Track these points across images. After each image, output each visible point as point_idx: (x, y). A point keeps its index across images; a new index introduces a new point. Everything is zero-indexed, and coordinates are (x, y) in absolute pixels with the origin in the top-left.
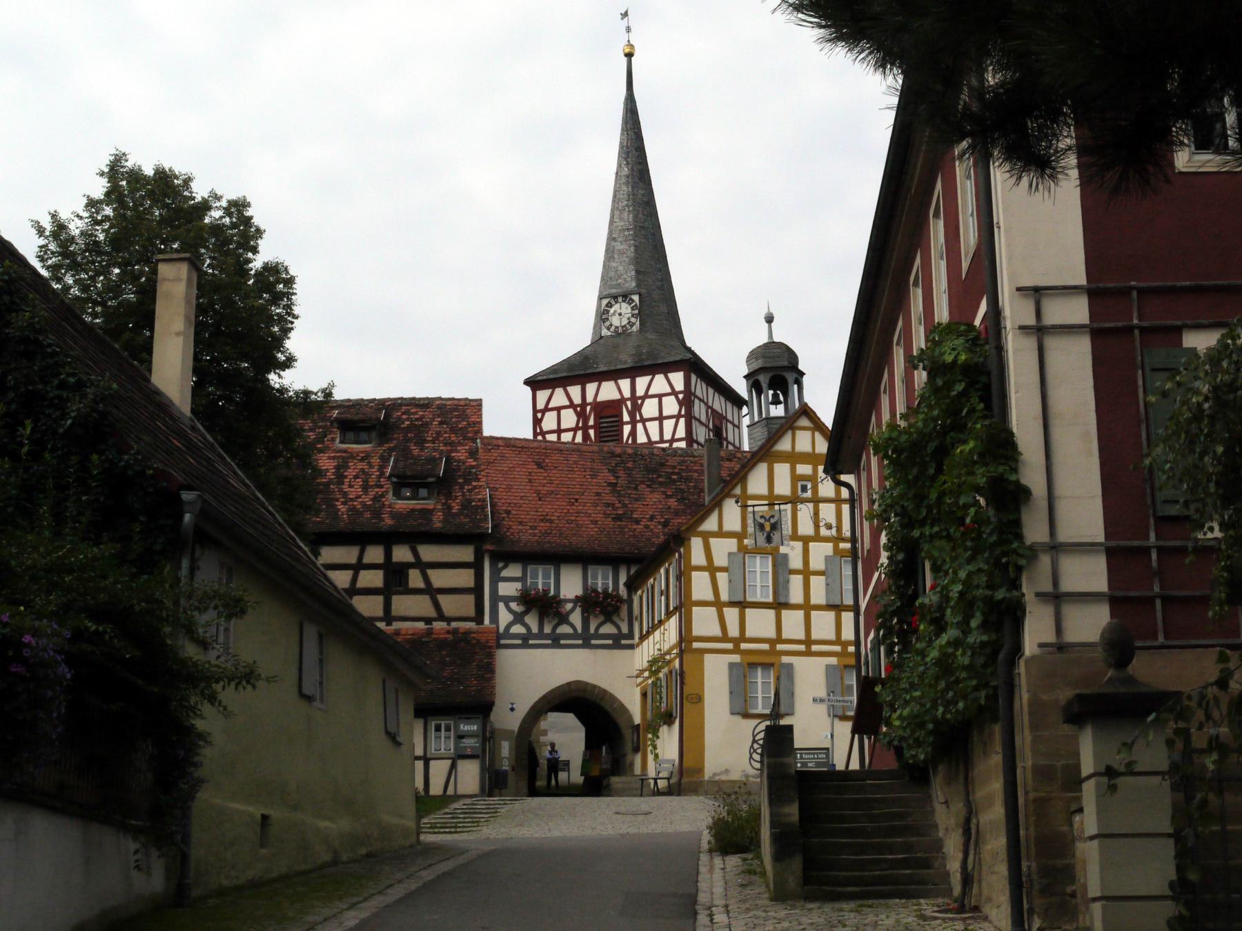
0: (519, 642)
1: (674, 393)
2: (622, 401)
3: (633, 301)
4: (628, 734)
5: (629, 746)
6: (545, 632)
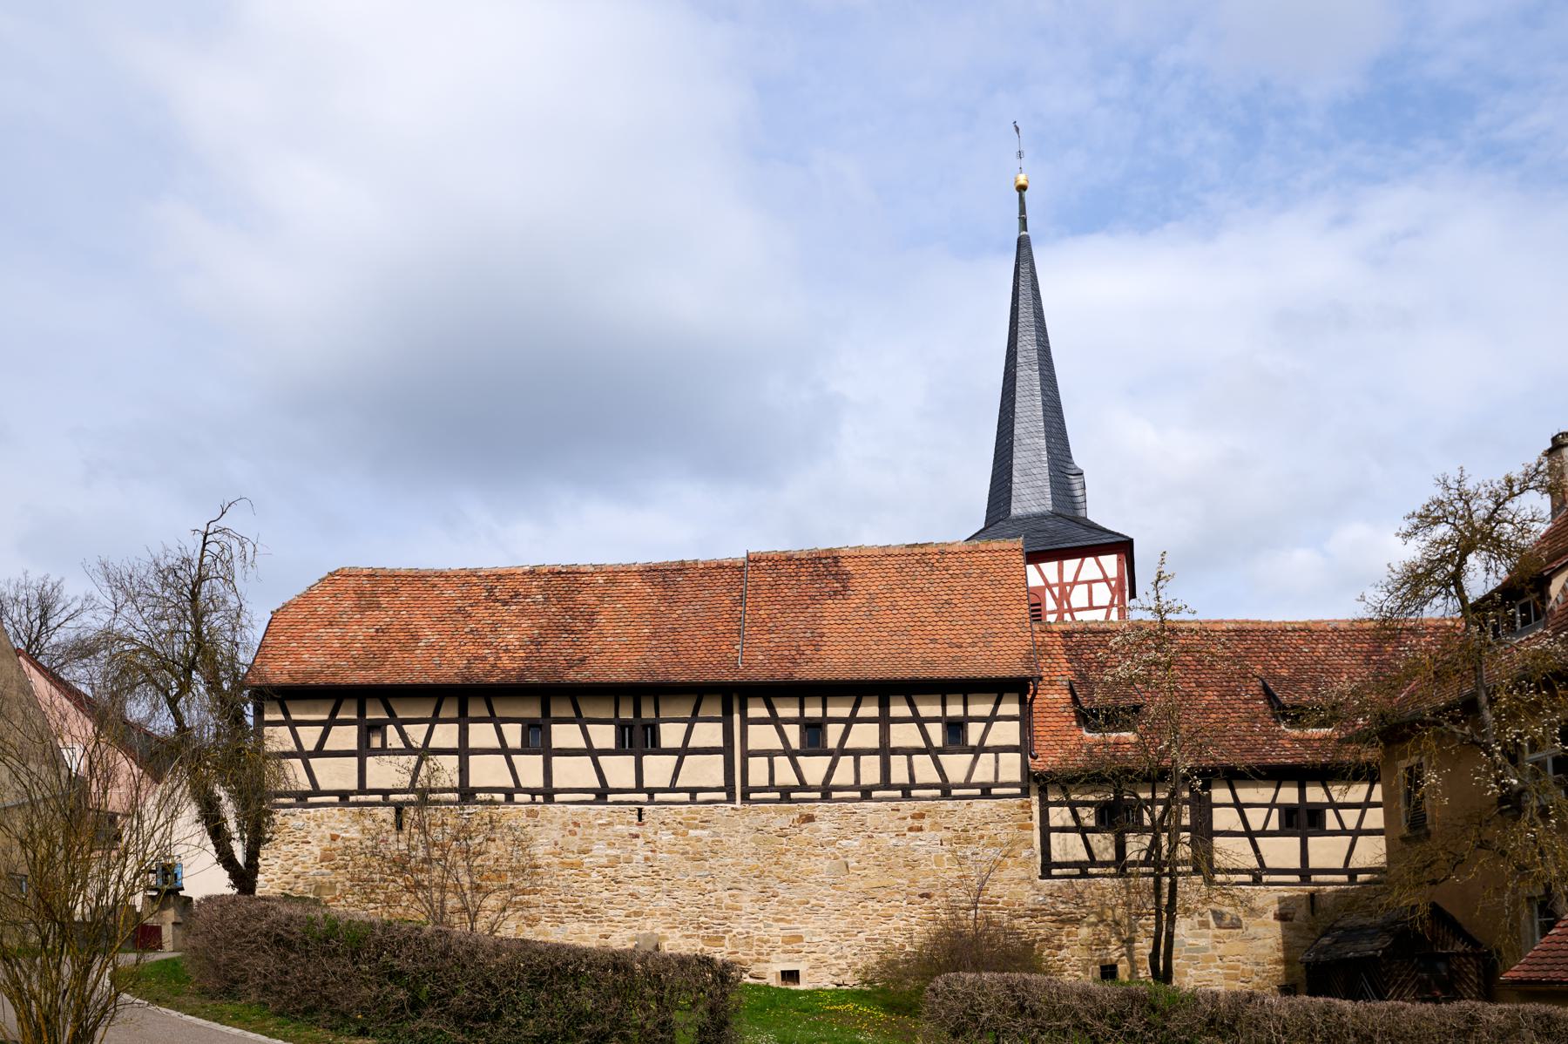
1: (1106, 580)
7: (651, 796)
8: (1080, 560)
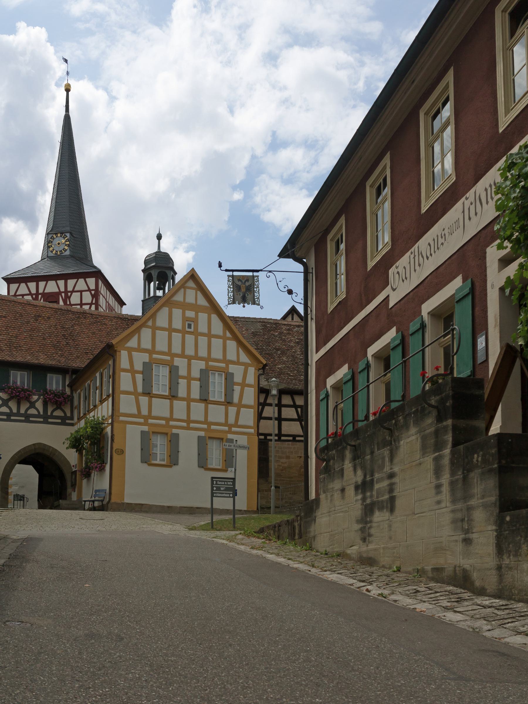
0: (5, 417)
1: (89, 290)
2: (60, 293)
3: (67, 237)
4: (68, 477)
5: (69, 484)
6: (21, 412)
7: (209, 426)
8: (17, 285)
